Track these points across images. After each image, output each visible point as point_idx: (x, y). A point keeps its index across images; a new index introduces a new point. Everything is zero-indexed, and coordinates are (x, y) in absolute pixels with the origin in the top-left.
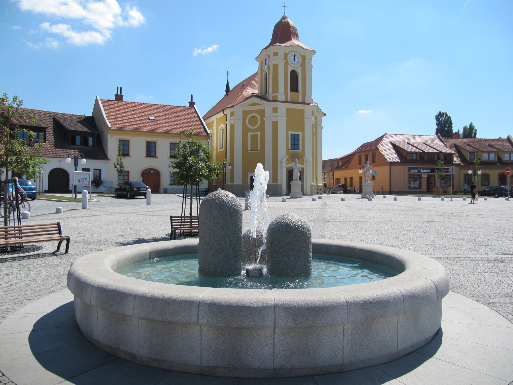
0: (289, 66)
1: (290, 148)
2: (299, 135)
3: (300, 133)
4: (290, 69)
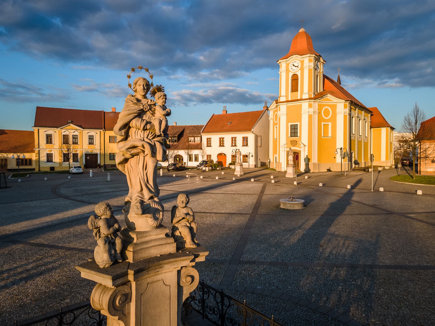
0: (290, 73)
1: (289, 136)
2: (291, 125)
3: (298, 123)
4: (291, 74)
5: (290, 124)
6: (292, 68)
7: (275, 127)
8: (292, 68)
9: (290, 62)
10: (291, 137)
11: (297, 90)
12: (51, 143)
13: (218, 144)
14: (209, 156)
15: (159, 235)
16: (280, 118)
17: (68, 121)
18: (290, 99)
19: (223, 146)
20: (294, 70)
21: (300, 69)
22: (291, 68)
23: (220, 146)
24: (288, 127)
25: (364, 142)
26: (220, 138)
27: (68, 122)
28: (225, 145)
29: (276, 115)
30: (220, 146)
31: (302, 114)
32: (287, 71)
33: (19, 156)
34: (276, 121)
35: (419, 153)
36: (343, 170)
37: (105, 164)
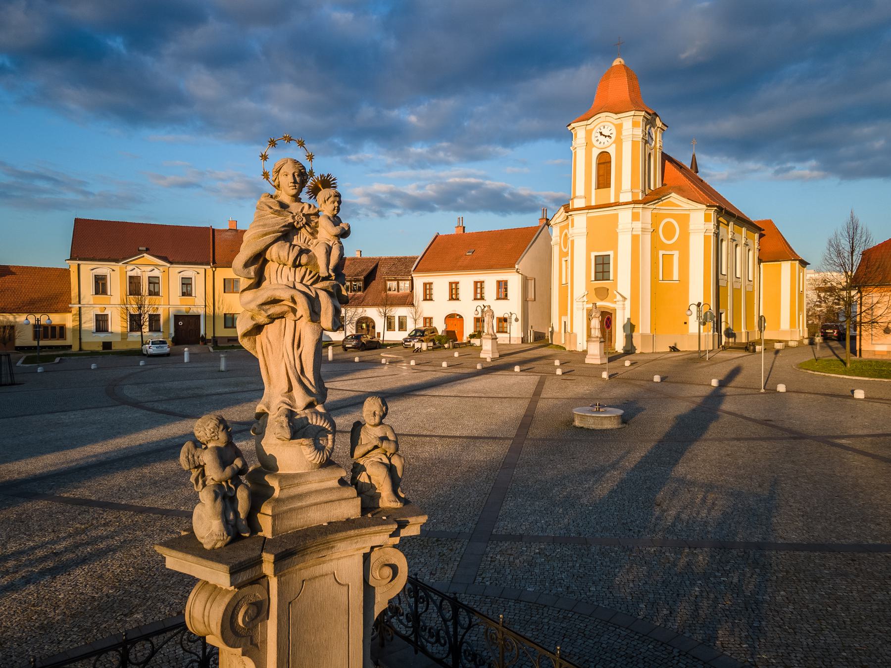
0: (594, 149)
1: (593, 279)
2: (596, 256)
3: (611, 253)
4: (595, 153)
5: (593, 254)
6: (597, 140)
7: (564, 259)
8: (597, 140)
9: (594, 128)
10: (596, 280)
11: (608, 185)
12: (104, 292)
13: (447, 296)
14: (428, 320)
15: (326, 482)
16: (573, 241)
17: (140, 248)
18: (593, 204)
19: (458, 299)
20: (602, 143)
21: (614, 142)
22: (597, 139)
23: (451, 299)
24: (590, 260)
25: (746, 292)
26: (451, 284)
27: (139, 250)
28: (461, 296)
29: (566, 235)
30: (451, 299)
31: (619, 234)
32: (589, 145)
33: (38, 319)
34: (565, 248)
35: (858, 313)
36: (702, 349)
37: (216, 335)
